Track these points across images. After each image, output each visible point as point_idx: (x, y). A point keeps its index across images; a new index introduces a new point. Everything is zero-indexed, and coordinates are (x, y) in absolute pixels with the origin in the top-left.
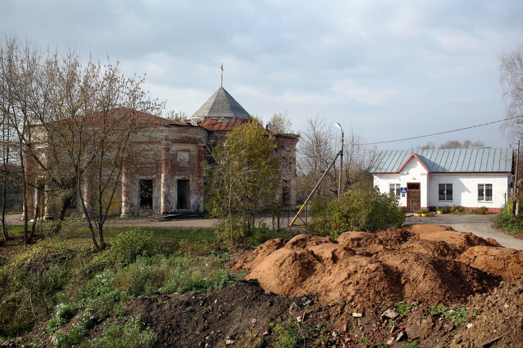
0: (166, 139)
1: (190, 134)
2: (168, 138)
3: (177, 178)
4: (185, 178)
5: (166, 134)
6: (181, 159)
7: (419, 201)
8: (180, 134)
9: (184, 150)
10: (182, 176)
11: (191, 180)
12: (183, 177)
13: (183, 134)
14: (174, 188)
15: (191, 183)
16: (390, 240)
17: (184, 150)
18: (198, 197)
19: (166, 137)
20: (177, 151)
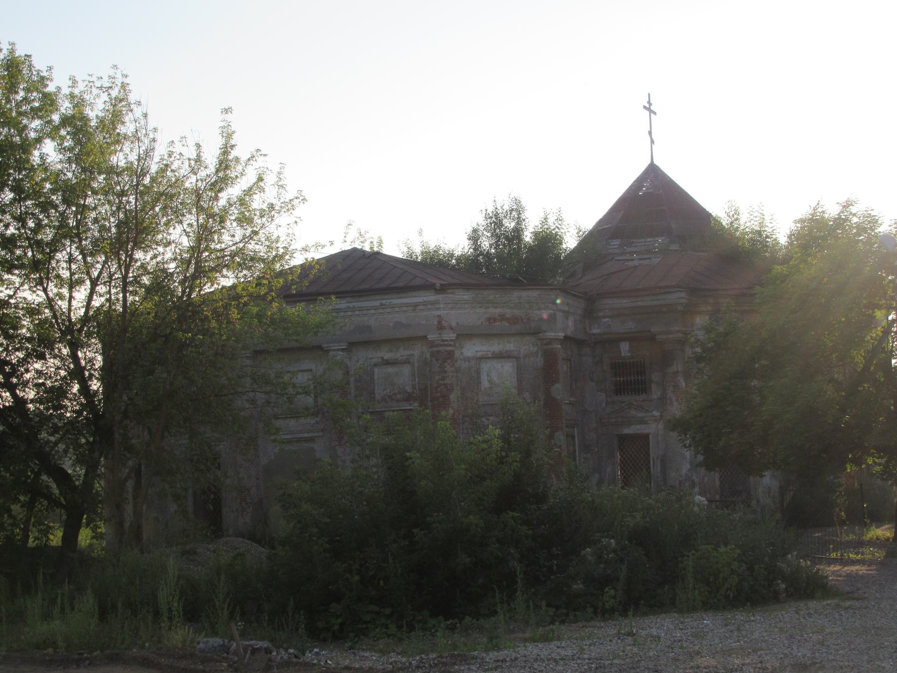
2: (444, 324)
8: (483, 310)
17: (499, 356)
19: (440, 322)
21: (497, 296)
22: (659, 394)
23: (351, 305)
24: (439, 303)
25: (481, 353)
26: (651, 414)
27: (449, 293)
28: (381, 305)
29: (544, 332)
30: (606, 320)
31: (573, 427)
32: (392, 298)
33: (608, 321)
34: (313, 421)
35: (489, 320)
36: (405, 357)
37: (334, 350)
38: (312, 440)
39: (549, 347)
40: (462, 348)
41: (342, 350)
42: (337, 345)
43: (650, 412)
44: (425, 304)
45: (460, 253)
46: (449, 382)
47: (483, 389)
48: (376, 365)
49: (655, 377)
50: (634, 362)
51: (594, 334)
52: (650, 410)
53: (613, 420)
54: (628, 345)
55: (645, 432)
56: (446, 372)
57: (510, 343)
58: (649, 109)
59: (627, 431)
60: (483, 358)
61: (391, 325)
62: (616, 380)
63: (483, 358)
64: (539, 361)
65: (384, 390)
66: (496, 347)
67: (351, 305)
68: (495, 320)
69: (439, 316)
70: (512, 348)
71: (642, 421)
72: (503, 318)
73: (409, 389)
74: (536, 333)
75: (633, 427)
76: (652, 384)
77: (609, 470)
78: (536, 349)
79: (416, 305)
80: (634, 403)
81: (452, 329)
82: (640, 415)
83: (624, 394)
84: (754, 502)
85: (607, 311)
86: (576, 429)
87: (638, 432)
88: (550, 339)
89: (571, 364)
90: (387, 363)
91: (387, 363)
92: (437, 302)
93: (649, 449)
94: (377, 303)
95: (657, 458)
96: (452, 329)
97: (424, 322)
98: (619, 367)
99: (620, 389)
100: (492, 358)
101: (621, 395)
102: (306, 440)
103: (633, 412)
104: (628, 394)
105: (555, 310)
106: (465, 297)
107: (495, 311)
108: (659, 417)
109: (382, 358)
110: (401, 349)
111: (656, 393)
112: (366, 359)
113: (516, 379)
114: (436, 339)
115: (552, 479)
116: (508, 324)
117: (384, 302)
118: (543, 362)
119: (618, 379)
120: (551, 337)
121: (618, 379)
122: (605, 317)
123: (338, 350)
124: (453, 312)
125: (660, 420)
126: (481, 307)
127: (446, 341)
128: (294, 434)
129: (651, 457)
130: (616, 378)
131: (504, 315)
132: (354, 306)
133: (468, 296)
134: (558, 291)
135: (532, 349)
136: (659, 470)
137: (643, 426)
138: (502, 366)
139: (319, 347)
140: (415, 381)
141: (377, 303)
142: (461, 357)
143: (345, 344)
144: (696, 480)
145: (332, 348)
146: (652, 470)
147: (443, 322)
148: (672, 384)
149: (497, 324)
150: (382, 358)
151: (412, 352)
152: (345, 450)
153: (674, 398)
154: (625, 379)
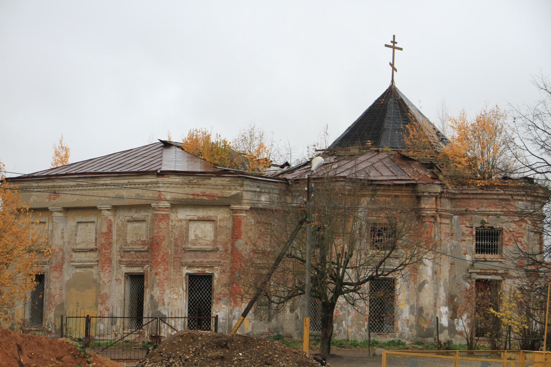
3: (186, 271)
6: (196, 236)
14: (181, 289)
23: (113, 182)
24: (159, 183)
27: (166, 177)
32: (135, 179)
38: (91, 267)
40: (177, 213)
41: (108, 210)
44: (152, 183)
45: (474, 121)
56: (160, 228)
64: (230, 224)
65: (132, 237)
67: (113, 182)
70: (212, 215)
79: (147, 184)
83: (489, 254)
92: (157, 183)
94: (126, 181)
101: (492, 254)
105: (242, 191)
106: (177, 180)
109: (132, 216)
110: (142, 211)
123: (105, 210)
131: (205, 193)
133: (178, 180)
135: (226, 215)
138: (205, 226)
139: (94, 208)
141: (126, 181)
150: (132, 216)
152: (105, 274)
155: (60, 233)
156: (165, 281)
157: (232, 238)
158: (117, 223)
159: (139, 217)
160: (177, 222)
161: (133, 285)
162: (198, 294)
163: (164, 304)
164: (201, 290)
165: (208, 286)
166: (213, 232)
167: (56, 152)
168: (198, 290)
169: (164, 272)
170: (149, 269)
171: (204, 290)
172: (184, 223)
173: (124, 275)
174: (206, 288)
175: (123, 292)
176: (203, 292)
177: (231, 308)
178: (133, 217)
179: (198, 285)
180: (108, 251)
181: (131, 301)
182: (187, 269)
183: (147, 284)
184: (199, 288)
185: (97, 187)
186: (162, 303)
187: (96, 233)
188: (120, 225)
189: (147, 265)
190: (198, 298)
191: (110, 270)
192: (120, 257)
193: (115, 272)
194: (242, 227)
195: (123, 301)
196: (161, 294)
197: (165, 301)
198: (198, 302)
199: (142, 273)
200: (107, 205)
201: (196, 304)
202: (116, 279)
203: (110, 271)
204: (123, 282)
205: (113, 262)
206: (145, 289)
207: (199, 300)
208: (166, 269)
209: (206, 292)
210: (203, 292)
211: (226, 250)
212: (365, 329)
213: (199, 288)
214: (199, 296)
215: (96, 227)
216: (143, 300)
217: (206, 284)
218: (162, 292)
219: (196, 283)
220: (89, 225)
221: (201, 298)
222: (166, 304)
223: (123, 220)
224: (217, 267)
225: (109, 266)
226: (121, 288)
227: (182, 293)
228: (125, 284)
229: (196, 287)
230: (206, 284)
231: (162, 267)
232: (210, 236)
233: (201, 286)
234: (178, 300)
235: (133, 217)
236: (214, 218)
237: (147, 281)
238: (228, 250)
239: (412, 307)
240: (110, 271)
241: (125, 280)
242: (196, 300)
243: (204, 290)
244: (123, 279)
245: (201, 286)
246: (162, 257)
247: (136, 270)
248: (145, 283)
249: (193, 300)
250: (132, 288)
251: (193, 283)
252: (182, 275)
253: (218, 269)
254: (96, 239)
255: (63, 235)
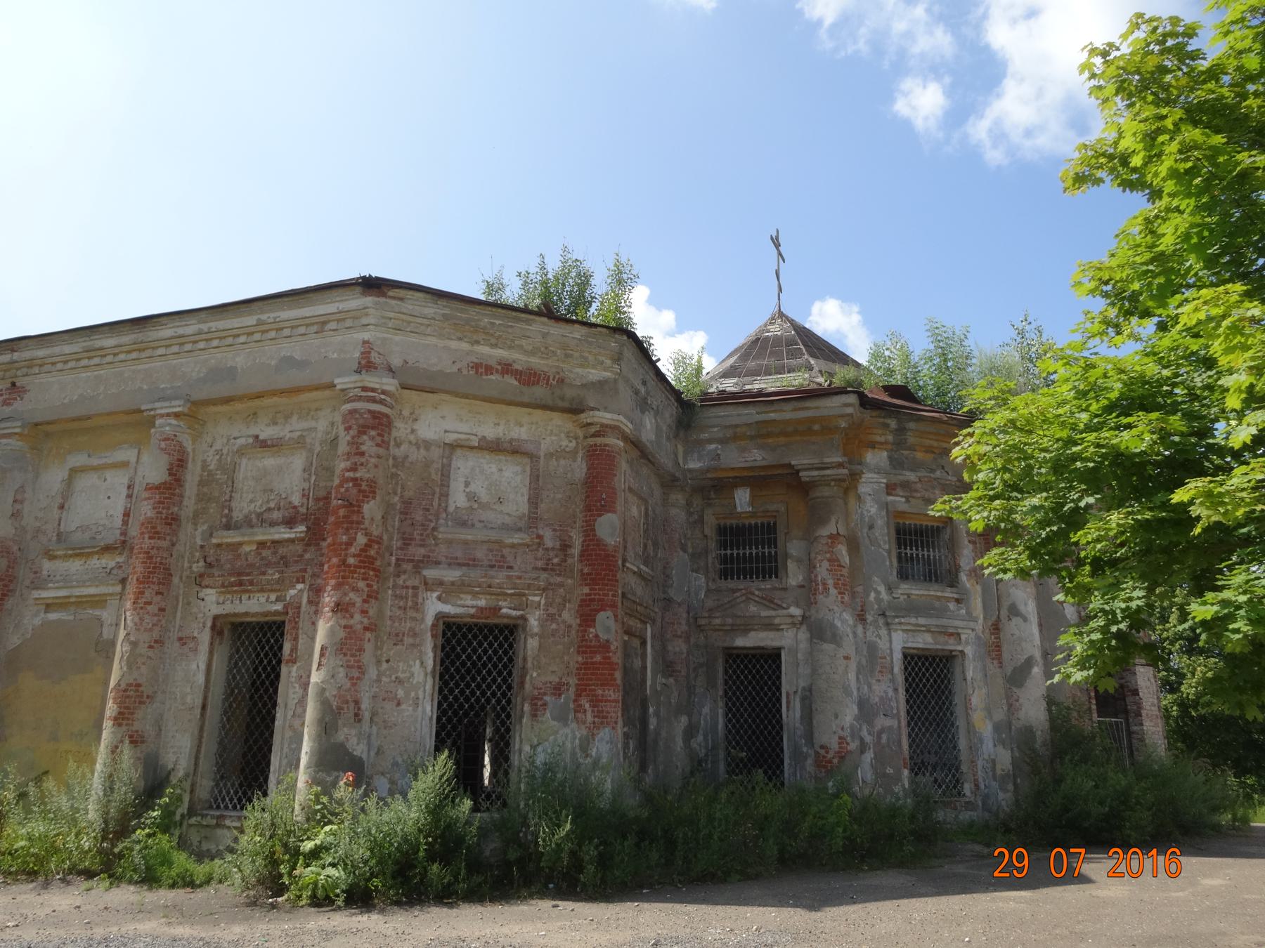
0: (366, 365)
1: (532, 353)
2: (374, 357)
3: (434, 606)
4: (496, 610)
5: (366, 336)
6: (472, 497)
7: (339, 377)
8: (465, 346)
9: (494, 447)
10: (475, 595)
11: (533, 623)
12: (482, 603)
13: (485, 350)
14: (416, 668)
15: (532, 644)
16: (999, 471)
17: (494, 447)
18: (581, 732)
19: (366, 354)
20: (453, 447)
21: (498, 322)
22: (801, 578)
23: (204, 327)
25: (455, 436)
26: (785, 612)
28: (260, 323)
29: (592, 409)
30: (713, 446)
31: (645, 623)
33: (717, 448)
34: (112, 564)
35: (476, 367)
36: (298, 434)
37: (162, 416)
38: (99, 602)
39: (599, 440)
42: (166, 404)
43: (784, 608)
46: (367, 476)
47: (451, 509)
48: (241, 452)
49: (795, 548)
50: (756, 524)
51: (690, 471)
52: (784, 605)
53: (718, 621)
54: (748, 495)
55: (776, 644)
56: (362, 454)
57: (521, 426)
58: (776, 242)
59: (740, 642)
60: (462, 446)
61: (273, 363)
62: (726, 555)
63: (462, 446)
64: (579, 469)
65: (251, 501)
66: (490, 426)
67: (204, 327)
68: (489, 370)
69: (365, 342)
70: (524, 437)
71: (770, 626)
72: (506, 368)
73: (296, 499)
74: (575, 410)
75: (752, 634)
76: (789, 561)
77: (706, 710)
78: (573, 444)
80: (757, 593)
81: (390, 370)
82: (765, 613)
84: (967, 788)
85: (716, 429)
86: (648, 626)
87: (762, 644)
88: (602, 425)
89: (647, 509)
90: (263, 445)
91: (263, 445)
93: (779, 678)
95: (795, 692)
96: (390, 370)
97: (335, 355)
98: (732, 535)
99: (731, 568)
100: (480, 448)
102: (83, 602)
103: (753, 608)
104: (745, 578)
107: (488, 352)
108: (800, 619)
109: (257, 437)
111: (794, 576)
112: (229, 440)
113: (526, 498)
114: (352, 386)
115: (585, 711)
116: (516, 383)
117: (264, 317)
118: (585, 470)
119: (729, 552)
120: (605, 421)
121: (729, 552)
122: (710, 441)
123: (168, 415)
124: (397, 338)
125: (801, 624)
126: (460, 339)
127: (373, 390)
128: (72, 587)
129: (784, 691)
130: (726, 549)
132: (210, 328)
134: (625, 338)
136: (798, 714)
137: (771, 634)
138: (501, 470)
140: (309, 480)
142: (412, 437)
143: (181, 402)
144: (868, 739)
145: (159, 412)
146: (784, 716)
147: (373, 354)
148: (828, 555)
149: (493, 377)
150: (257, 437)
151: (313, 424)
153: (830, 582)
154: (741, 552)
155: (10, 500)
156: (368, 635)
157: (588, 509)
158: (204, 461)
159: (281, 434)
160: (414, 449)
161: (241, 658)
162: (468, 685)
163: (358, 717)
164: (479, 672)
165: (500, 659)
166: (525, 491)
167: (248, 905)
168: (468, 671)
169: (365, 601)
170: (305, 600)
171: (489, 673)
172: (436, 453)
173: (209, 624)
174: (495, 666)
175: (201, 679)
176: (484, 679)
177: (584, 732)
178: (261, 438)
179: (469, 658)
180: (165, 544)
181: (225, 713)
182: (439, 598)
183: (294, 649)
184: (474, 664)
185: (148, 353)
186: (351, 715)
187: (129, 496)
188: (212, 467)
189: (300, 586)
190: (467, 700)
191: (163, 605)
192: (202, 563)
193: (179, 614)
194: (616, 479)
195: (198, 711)
196: (352, 678)
197: (363, 706)
198: (466, 714)
199: (277, 613)
200: (176, 398)
201: (460, 721)
202: (180, 639)
203: (162, 610)
204: (204, 648)
205: (176, 580)
206: (284, 669)
207: (472, 707)
208: (372, 596)
209: (494, 680)
210: (484, 679)
211: (565, 547)
212: (904, 789)
213: (474, 664)
214: (473, 693)
215: (131, 479)
216: (275, 705)
217: (495, 652)
218: (357, 675)
219: (464, 650)
220: (109, 474)
221: (478, 700)
222: (367, 715)
223: (225, 451)
224: (537, 599)
225: (158, 593)
226: (194, 666)
227: (421, 679)
228: (211, 653)
229: (463, 664)
230: (495, 652)
231: (361, 584)
232: (518, 504)
233: (480, 658)
234: (403, 707)
235: (261, 438)
236: (530, 447)
237: (296, 639)
238: (570, 547)
239: (997, 728)
240: (162, 610)
241: (212, 638)
242: (461, 706)
243: (489, 673)
244: (205, 637)
245: (480, 658)
246: (362, 550)
247: (256, 605)
248: (287, 647)
249: (450, 705)
250: (233, 667)
251: (453, 649)
252: (423, 620)
253: (539, 603)
254: (127, 514)
255: (18, 506)
